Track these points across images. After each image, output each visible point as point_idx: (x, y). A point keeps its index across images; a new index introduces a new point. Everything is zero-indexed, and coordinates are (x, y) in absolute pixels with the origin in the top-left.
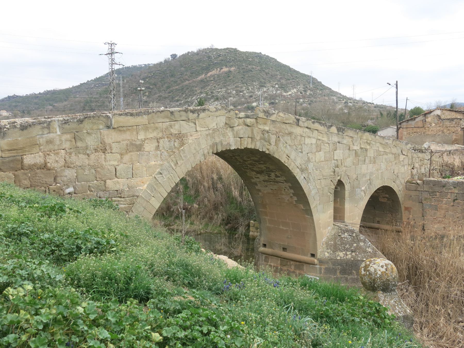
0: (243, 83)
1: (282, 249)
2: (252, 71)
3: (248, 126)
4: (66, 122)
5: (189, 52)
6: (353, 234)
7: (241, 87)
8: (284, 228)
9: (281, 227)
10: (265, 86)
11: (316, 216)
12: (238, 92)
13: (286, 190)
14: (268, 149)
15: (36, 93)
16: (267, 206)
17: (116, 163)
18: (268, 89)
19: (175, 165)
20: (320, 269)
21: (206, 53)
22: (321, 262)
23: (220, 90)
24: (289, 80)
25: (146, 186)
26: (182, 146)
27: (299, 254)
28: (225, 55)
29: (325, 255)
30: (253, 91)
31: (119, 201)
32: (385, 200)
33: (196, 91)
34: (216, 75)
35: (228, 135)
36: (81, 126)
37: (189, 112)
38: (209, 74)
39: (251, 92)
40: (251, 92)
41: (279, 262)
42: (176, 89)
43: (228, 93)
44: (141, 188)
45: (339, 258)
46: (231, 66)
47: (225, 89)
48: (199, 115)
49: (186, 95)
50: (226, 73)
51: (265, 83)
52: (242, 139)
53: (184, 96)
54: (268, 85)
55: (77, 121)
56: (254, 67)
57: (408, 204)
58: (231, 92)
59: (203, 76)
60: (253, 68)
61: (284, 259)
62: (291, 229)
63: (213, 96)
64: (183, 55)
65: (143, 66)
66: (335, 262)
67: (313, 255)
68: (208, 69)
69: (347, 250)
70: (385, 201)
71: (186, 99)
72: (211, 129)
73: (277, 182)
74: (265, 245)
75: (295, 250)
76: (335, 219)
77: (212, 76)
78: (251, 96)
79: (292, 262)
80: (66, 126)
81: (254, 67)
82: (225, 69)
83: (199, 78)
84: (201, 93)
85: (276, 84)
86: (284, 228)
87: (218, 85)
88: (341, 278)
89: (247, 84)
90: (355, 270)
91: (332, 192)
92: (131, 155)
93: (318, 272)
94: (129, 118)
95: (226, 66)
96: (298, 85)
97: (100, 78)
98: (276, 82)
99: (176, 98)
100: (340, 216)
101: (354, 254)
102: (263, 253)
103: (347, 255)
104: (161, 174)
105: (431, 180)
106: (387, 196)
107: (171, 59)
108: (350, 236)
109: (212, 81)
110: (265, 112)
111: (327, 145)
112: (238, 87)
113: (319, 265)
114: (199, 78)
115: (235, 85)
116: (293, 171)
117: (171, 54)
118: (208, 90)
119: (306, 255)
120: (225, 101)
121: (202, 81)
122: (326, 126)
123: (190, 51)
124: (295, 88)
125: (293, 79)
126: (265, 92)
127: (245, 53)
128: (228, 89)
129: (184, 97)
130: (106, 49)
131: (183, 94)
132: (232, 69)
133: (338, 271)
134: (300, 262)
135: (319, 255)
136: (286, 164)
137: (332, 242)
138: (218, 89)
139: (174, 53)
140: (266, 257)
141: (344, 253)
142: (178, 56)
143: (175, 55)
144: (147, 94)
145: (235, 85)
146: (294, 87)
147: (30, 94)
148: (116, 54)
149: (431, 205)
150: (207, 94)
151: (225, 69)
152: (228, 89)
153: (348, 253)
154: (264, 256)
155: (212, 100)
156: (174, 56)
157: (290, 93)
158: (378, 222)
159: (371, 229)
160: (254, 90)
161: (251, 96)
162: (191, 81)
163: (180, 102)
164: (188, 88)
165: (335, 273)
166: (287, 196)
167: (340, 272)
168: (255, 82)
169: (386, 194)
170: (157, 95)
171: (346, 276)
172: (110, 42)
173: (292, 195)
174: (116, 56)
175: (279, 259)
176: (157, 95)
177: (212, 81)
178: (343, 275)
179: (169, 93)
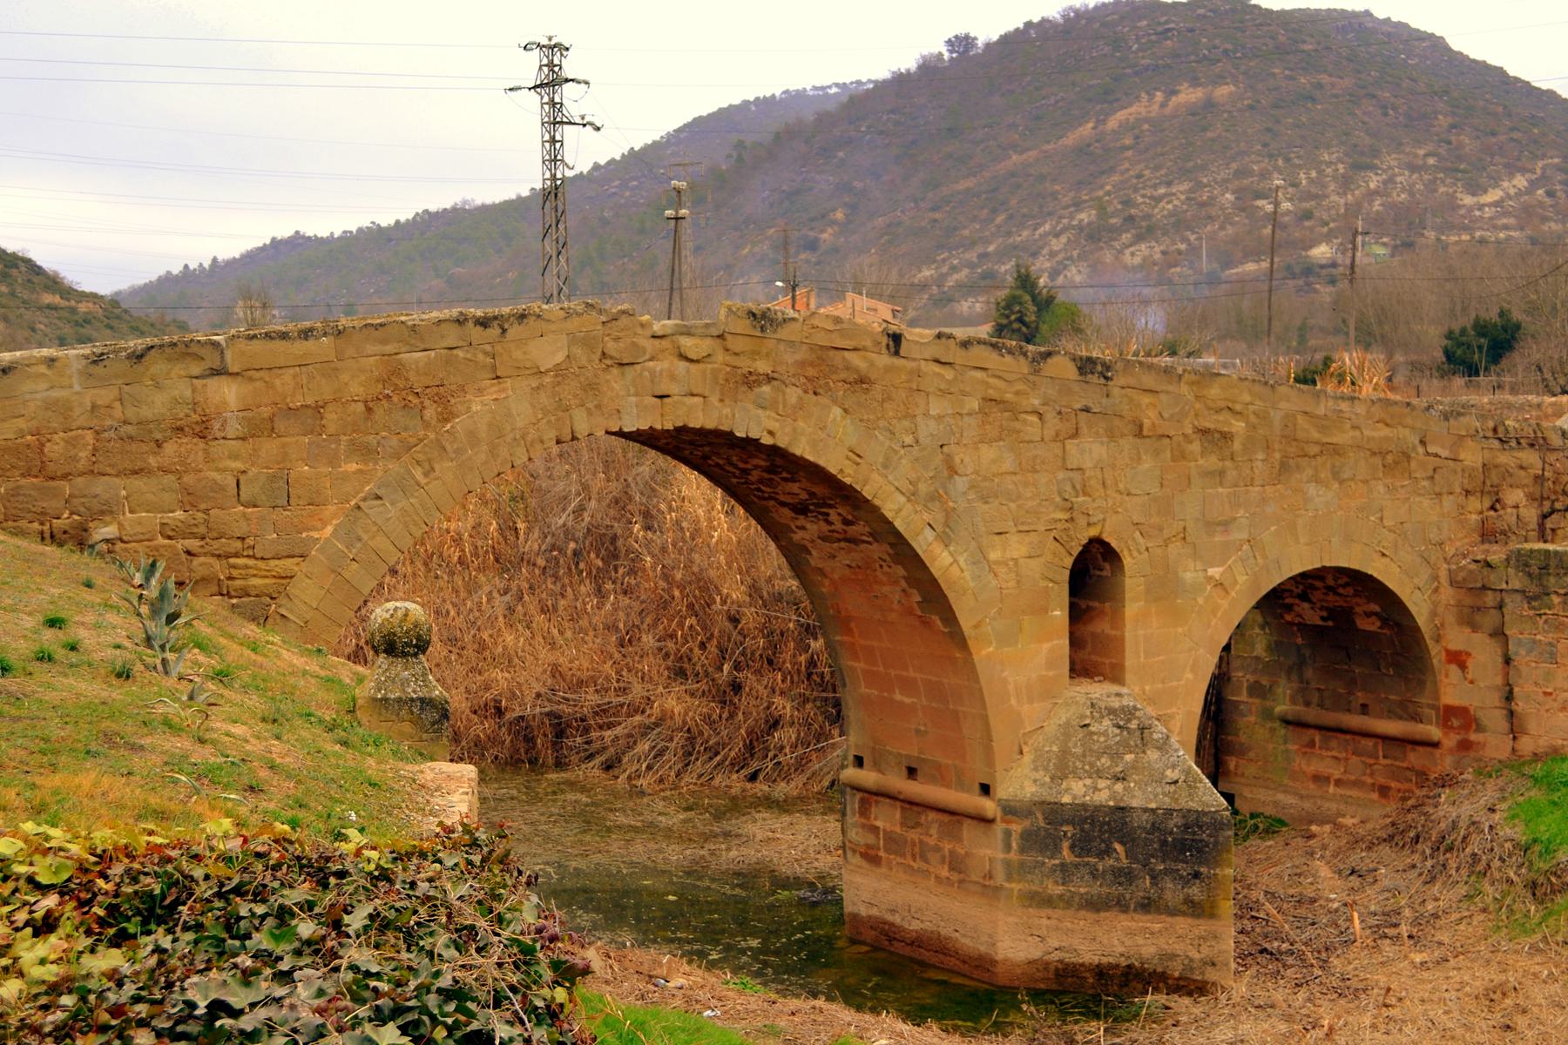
0: (1271, 156)
1: (905, 772)
2: (1313, 100)
3: (692, 361)
4: (98, 359)
5: (1029, 25)
6: (1129, 721)
7: (1264, 175)
8: (907, 700)
9: (898, 697)
10: (1373, 168)
11: (984, 653)
12: (1247, 197)
13: (886, 568)
14: (771, 433)
15: (384, 224)
16: (853, 625)
17: (238, 465)
18: (1391, 180)
19: (426, 475)
20: (1008, 834)
21: (1104, 25)
22: (1011, 810)
23: (1162, 191)
24: (1493, 134)
25: (329, 529)
26: (447, 420)
27: (948, 786)
28: (1191, 30)
29: (1022, 788)
30: (1314, 190)
31: (247, 567)
32: (1372, 625)
33: (1054, 195)
34: (1146, 120)
35: (612, 389)
36: (139, 368)
37: (471, 324)
38: (1112, 124)
39: (1310, 196)
40: (1310, 196)
41: (898, 815)
42: (968, 190)
43: (1203, 205)
44: (316, 535)
45: (1066, 799)
46: (1220, 79)
47: (1185, 186)
48: (504, 331)
49: (1011, 217)
50: (1192, 111)
51: (1376, 153)
52: (666, 400)
53: (1000, 219)
54: (1391, 160)
55: (128, 357)
56: (1325, 79)
57: (1457, 638)
58: (1212, 198)
59: (1087, 129)
60: (1320, 86)
61: (913, 805)
62: (924, 702)
63: (1131, 218)
64: (1006, 39)
65: (834, 90)
66: (1055, 813)
67: (986, 789)
68: (1109, 98)
69: (1099, 774)
70: (1373, 628)
71: (1009, 234)
72: (548, 371)
73: (854, 541)
74: (859, 762)
75: (940, 776)
76: (1080, 669)
77: (1126, 127)
78: (1308, 215)
79: (932, 815)
80: (99, 370)
81: (1325, 79)
82: (1189, 95)
83: (1070, 139)
84: (1078, 205)
85: (1426, 155)
86: (907, 700)
87: (1157, 168)
88: (1076, 866)
89: (1287, 160)
90: (1121, 843)
91: (1058, 578)
92: (284, 445)
93: (1000, 845)
94: (279, 345)
95: (1195, 82)
96: (1535, 157)
97: (647, 149)
98: (1430, 147)
99: (966, 232)
100: (1113, 666)
101: (1119, 787)
102: (857, 788)
103: (1096, 789)
104: (379, 498)
105: (1531, 551)
106: (1377, 609)
107: (946, 56)
108: (1119, 727)
109: (1128, 148)
110: (754, 315)
111: (1034, 419)
112: (1250, 173)
113: (1003, 821)
114: (1070, 139)
115: (1234, 166)
116: (877, 502)
117: (951, 35)
118: (1108, 193)
119: (961, 786)
120: (1184, 240)
121: (1082, 150)
122: (1025, 354)
123: (1035, 20)
124: (1523, 171)
125: (1512, 129)
126: (1376, 192)
127: (1282, 13)
128: (1200, 186)
129: (999, 227)
130: (529, 68)
131: (994, 211)
132: (1223, 91)
133: (1066, 845)
134: (952, 813)
135: (1004, 791)
136: (847, 480)
137: (1055, 748)
138: (1155, 187)
139: (961, 31)
140: (862, 800)
141: (1088, 782)
142: (980, 43)
143: (967, 37)
144: (839, 215)
145: (1234, 166)
146: (1512, 169)
147: (360, 230)
148: (566, 86)
149: (1534, 642)
150: (1102, 209)
151: (1189, 95)
152: (1200, 186)
153: (1102, 784)
154: (859, 796)
155: (1126, 237)
156: (962, 43)
157: (1493, 196)
158: (1364, 709)
159: (1342, 737)
160: (1324, 186)
161: (1308, 215)
162: (1033, 153)
163: (980, 249)
164: (1019, 186)
165: (1057, 849)
166: (894, 590)
167: (1072, 847)
168: (1328, 147)
169: (1369, 600)
170: (880, 221)
171: (1093, 860)
172: (545, 42)
173: (903, 584)
174: (568, 92)
175: (898, 804)
176: (880, 221)
177: (1128, 148)
178: (1079, 856)
179: (933, 210)
